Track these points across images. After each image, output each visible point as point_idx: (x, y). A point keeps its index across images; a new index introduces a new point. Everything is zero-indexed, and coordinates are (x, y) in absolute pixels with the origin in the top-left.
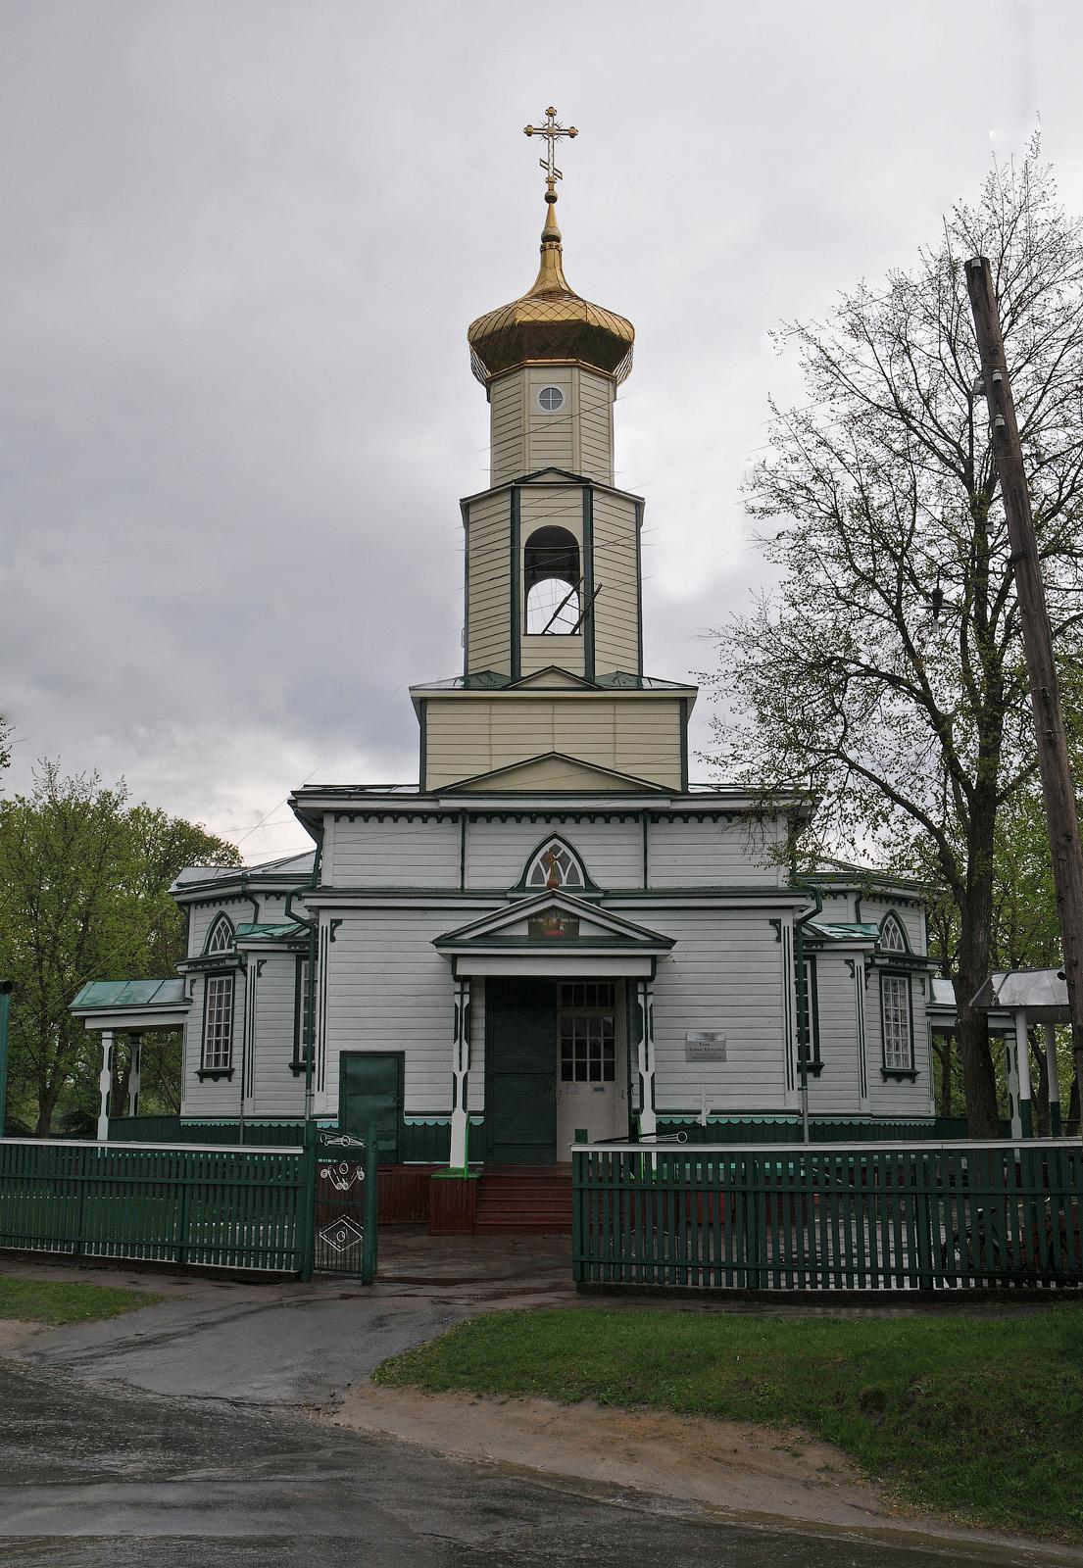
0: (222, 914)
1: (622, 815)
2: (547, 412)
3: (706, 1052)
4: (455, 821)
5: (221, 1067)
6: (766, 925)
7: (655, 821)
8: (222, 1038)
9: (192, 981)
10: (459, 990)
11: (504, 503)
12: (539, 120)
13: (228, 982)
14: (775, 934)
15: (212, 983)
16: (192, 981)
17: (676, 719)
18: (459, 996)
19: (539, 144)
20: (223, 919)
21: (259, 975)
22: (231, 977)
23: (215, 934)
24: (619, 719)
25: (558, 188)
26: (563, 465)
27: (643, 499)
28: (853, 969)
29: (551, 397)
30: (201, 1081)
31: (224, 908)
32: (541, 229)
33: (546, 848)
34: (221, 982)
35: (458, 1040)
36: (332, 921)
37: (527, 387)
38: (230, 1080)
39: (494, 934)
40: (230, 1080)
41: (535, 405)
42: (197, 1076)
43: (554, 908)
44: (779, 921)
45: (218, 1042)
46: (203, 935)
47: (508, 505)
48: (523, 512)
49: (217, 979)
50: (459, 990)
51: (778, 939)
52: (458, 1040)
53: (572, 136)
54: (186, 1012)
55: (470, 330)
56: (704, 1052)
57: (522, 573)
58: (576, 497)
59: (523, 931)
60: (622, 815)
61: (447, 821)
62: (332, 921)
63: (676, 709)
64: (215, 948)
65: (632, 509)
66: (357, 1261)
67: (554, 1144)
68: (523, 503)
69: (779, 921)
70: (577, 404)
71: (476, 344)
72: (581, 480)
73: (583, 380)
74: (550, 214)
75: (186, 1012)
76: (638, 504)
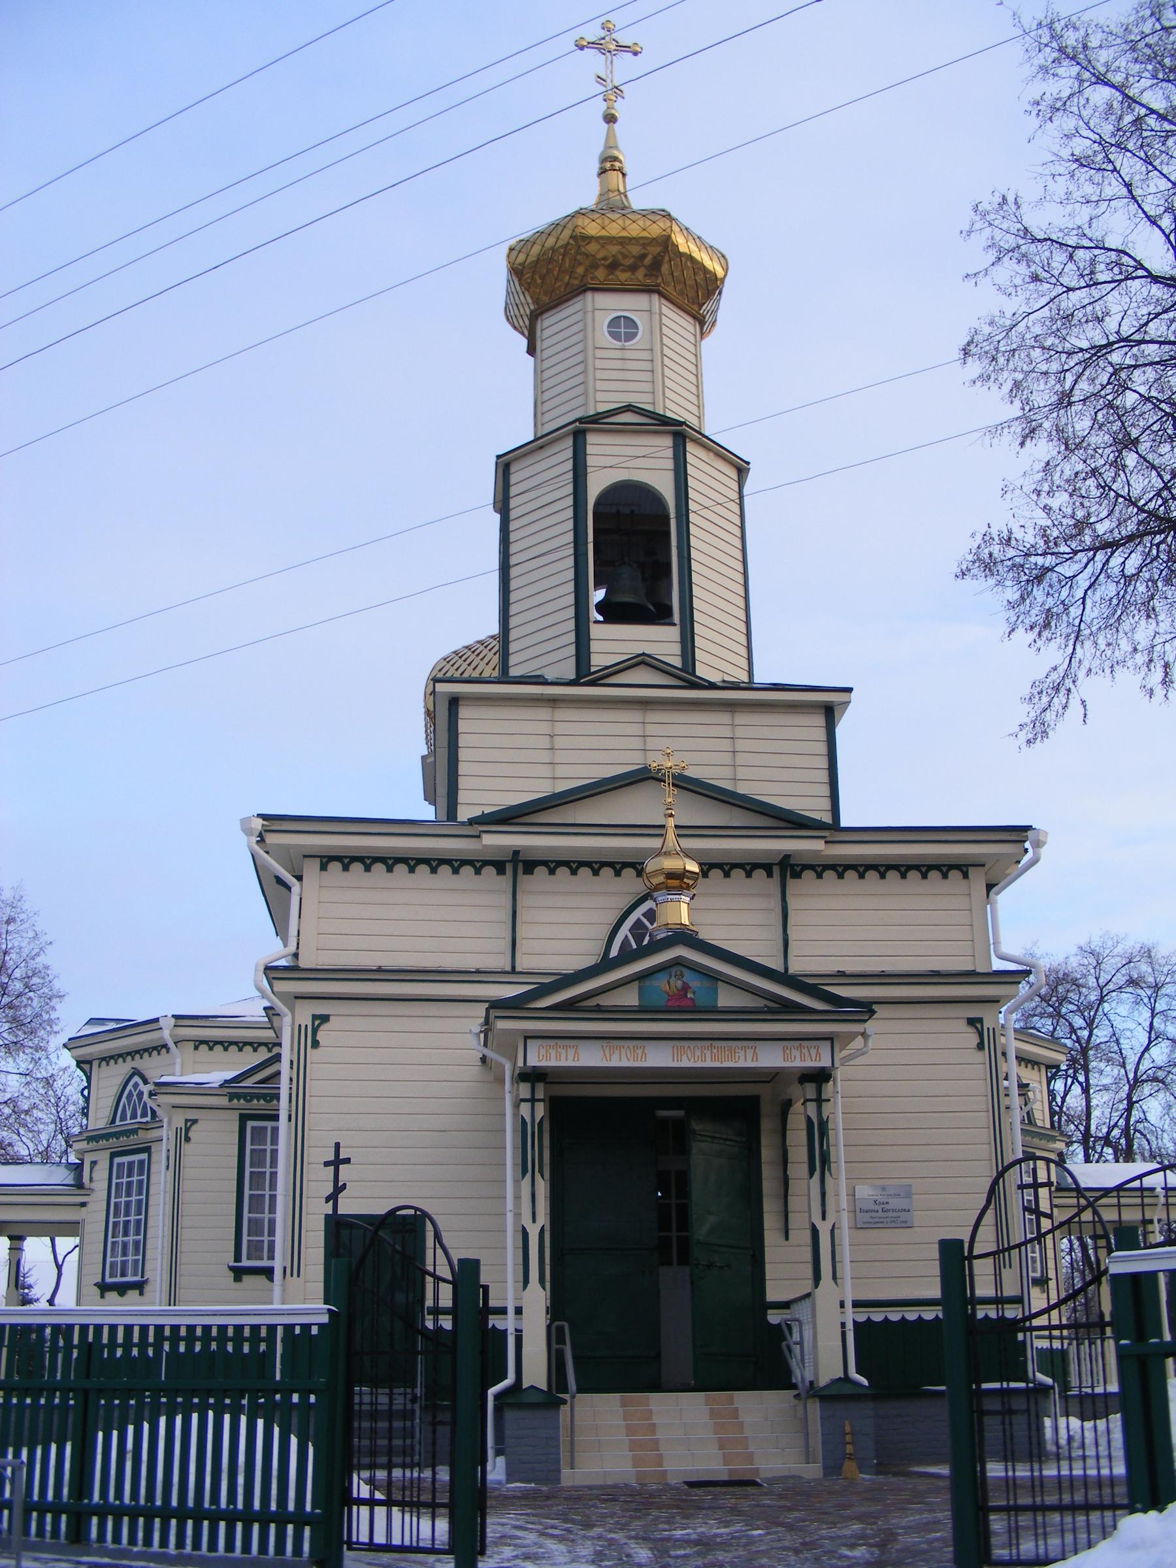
0: (136, 1072)
1: (750, 867)
2: (618, 344)
3: (885, 1214)
4: (770, 875)
5: (129, 1278)
6: (962, 1026)
7: (797, 875)
8: (131, 1238)
9: (92, 1162)
10: (528, 1096)
11: (564, 451)
12: (593, 32)
13: (141, 1162)
14: (974, 1039)
15: (119, 1165)
16: (92, 1162)
17: (821, 734)
18: (529, 1104)
19: (593, 61)
20: (136, 1079)
21: (188, 1139)
22: (144, 1156)
23: (124, 1099)
24: (740, 732)
25: (620, 109)
26: (642, 400)
27: (748, 463)
28: (981, 1035)
29: (623, 328)
30: (102, 1296)
31: (138, 1063)
32: (599, 148)
33: (638, 914)
34: (131, 1164)
35: (529, 1175)
36: (315, 1017)
37: (589, 315)
38: (141, 1294)
39: (592, 1002)
40: (141, 1294)
41: (603, 337)
42: (97, 1291)
43: (678, 962)
44: (980, 1020)
45: (125, 1245)
46: (110, 1102)
47: (569, 453)
48: (590, 461)
49: (125, 1159)
50: (528, 1096)
51: (980, 1046)
52: (529, 1175)
53: (635, 54)
54: (83, 1205)
55: (511, 249)
56: (880, 1214)
57: (591, 547)
58: (664, 445)
59: (629, 998)
60: (750, 867)
61: (760, 874)
62: (315, 1017)
63: (820, 720)
64: (123, 1118)
65: (733, 474)
66: (1091, 1452)
67: (658, 1356)
68: (590, 449)
69: (980, 1020)
70: (658, 328)
71: (518, 272)
72: (664, 421)
73: (665, 310)
74: (610, 136)
75: (83, 1205)
76: (742, 469)
